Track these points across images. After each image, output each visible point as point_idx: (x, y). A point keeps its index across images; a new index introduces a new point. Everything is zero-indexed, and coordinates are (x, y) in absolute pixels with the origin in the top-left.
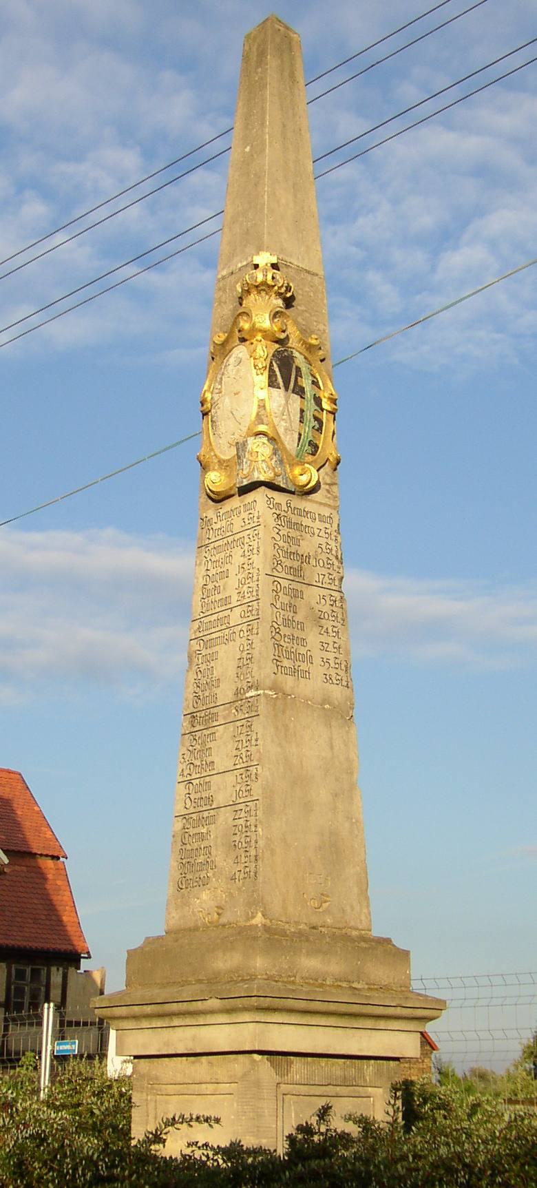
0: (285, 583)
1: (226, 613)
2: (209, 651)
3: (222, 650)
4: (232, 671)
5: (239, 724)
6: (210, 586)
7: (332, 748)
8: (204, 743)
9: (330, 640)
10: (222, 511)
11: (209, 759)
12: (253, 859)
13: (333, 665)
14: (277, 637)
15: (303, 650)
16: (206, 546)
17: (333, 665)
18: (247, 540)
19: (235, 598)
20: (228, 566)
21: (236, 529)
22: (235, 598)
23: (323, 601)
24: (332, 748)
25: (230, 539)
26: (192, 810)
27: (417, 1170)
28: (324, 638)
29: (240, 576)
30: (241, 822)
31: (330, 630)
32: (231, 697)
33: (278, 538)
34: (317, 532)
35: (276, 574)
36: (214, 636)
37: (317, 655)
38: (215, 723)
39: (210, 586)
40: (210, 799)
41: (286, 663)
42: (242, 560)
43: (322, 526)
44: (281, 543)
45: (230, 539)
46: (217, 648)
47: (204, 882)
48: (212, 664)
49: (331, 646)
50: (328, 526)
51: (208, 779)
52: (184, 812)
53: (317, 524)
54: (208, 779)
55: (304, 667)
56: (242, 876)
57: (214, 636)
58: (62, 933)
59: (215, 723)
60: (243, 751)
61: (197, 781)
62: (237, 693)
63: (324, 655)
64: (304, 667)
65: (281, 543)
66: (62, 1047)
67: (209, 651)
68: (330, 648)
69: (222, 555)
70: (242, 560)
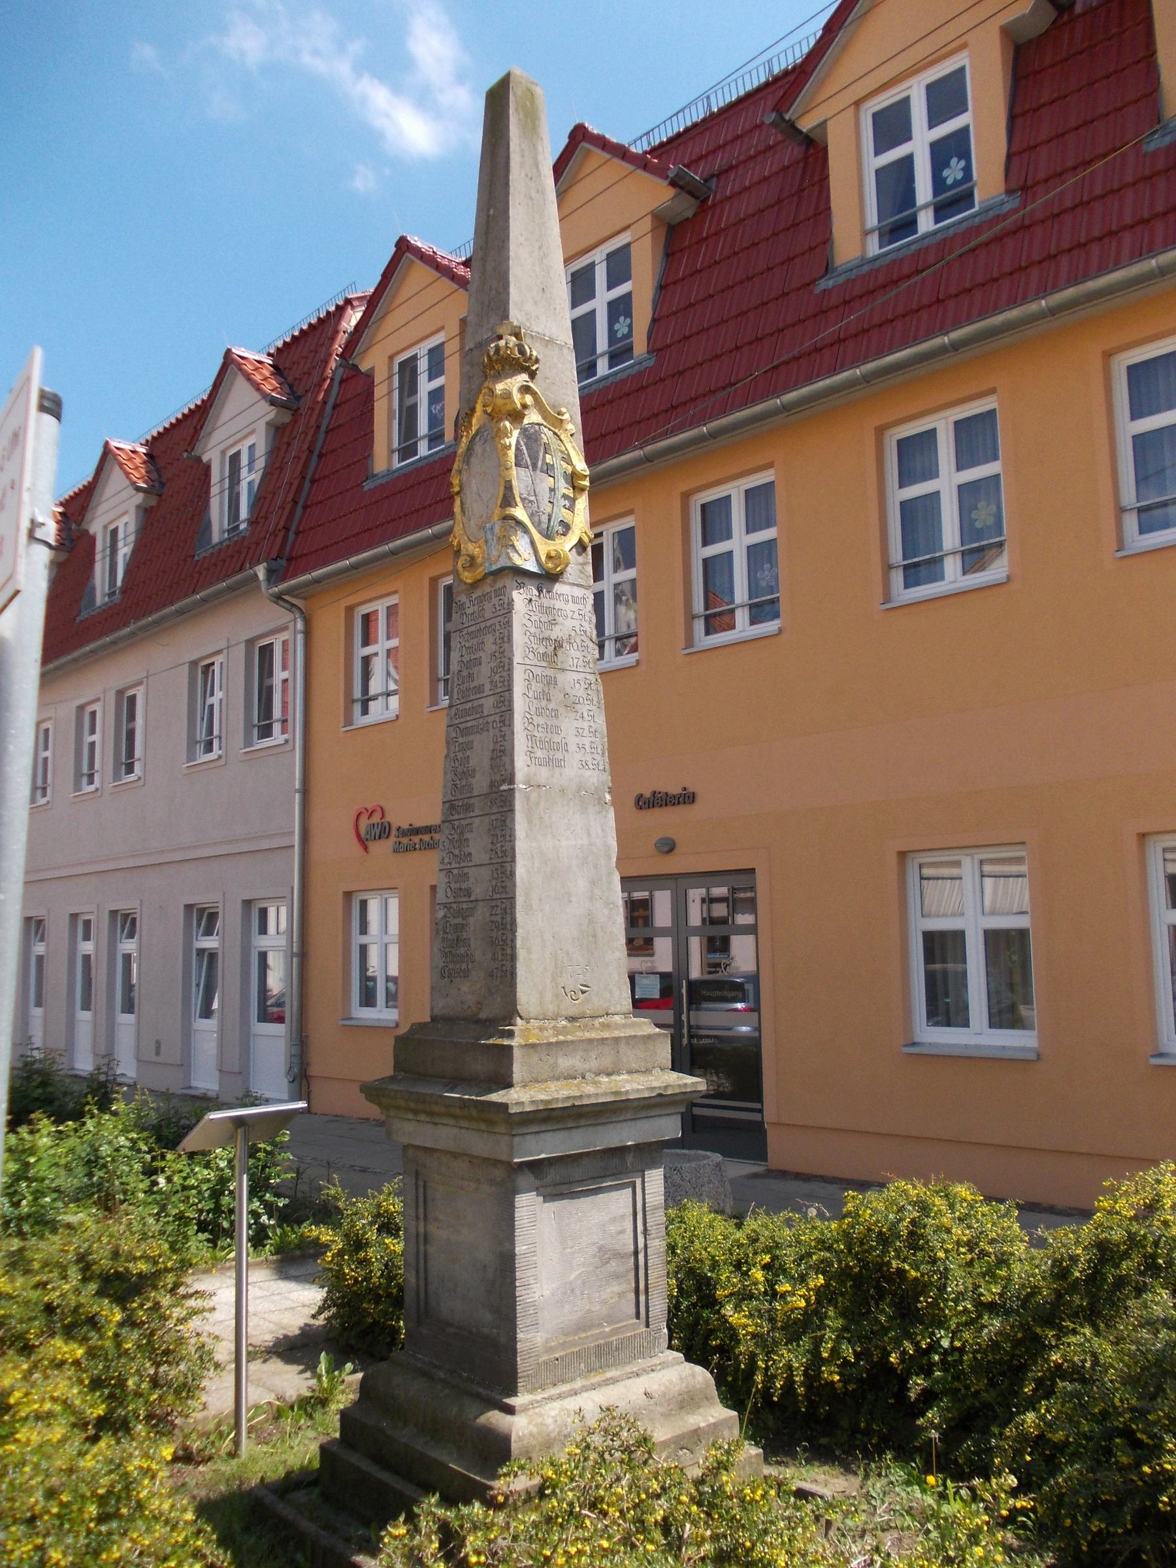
0: (538, 671)
1: (469, 821)
2: (465, 739)
3: (476, 739)
4: (486, 763)
5: (493, 817)
6: (465, 673)
7: (589, 834)
8: (462, 833)
9: (585, 725)
10: (474, 596)
11: (467, 850)
12: (509, 958)
13: (588, 749)
14: (530, 727)
15: (557, 739)
16: (460, 630)
17: (588, 749)
18: (498, 627)
19: (487, 686)
20: (481, 654)
21: (488, 615)
22: (487, 686)
23: (577, 686)
24: (589, 834)
25: (483, 625)
26: (452, 900)
27: (961, 1350)
28: (579, 724)
29: (492, 665)
30: (498, 918)
31: (585, 715)
32: (485, 790)
33: (529, 624)
34: (570, 614)
35: (528, 662)
36: (470, 724)
37: (573, 742)
38: (472, 814)
39: (465, 673)
40: (468, 892)
41: (539, 754)
42: (494, 648)
43: (575, 607)
44: (533, 630)
45: (483, 625)
46: (471, 738)
47: (466, 974)
48: (468, 753)
49: (586, 731)
50: (581, 607)
51: (466, 870)
52: (444, 900)
53: (571, 606)
54: (466, 870)
55: (559, 755)
56: (499, 974)
57: (470, 724)
58: (549, 1190)
59: (472, 814)
60: (499, 845)
61: (455, 871)
62: (492, 784)
63: (579, 740)
64: (559, 755)
65: (533, 630)
66: (571, 1062)
67: (465, 739)
68: (586, 733)
69: (475, 641)
70: (494, 648)
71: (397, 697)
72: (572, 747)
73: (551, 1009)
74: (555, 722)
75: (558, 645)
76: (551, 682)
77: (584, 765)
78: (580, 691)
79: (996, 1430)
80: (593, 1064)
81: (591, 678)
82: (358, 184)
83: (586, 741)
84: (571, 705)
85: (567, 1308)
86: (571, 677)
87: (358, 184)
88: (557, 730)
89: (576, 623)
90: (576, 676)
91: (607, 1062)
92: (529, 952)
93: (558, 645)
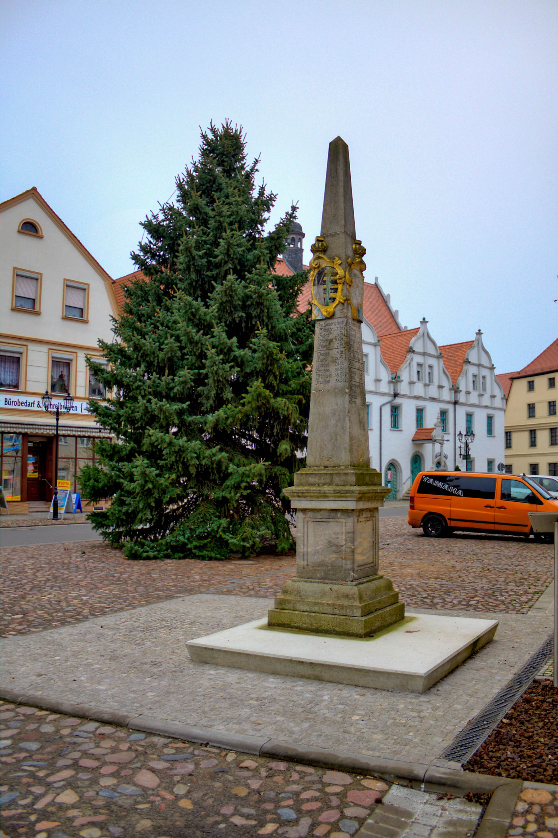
24: (337, 404)
37: (333, 373)
41: (321, 380)
64: (328, 379)
71: (426, 834)
72: (333, 375)
73: (318, 463)
74: (328, 368)
75: (331, 341)
76: (327, 355)
77: (337, 381)
78: (338, 355)
79: (161, 355)
80: (323, 481)
81: (343, 349)
82: (279, 256)
83: (339, 372)
84: (334, 361)
85: (316, 557)
86: (335, 351)
87: (279, 256)
88: (328, 370)
89: (339, 332)
90: (337, 350)
91: (328, 481)
92: (312, 445)
93: (331, 341)
